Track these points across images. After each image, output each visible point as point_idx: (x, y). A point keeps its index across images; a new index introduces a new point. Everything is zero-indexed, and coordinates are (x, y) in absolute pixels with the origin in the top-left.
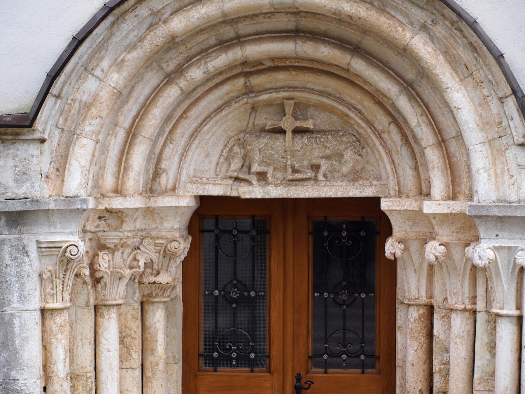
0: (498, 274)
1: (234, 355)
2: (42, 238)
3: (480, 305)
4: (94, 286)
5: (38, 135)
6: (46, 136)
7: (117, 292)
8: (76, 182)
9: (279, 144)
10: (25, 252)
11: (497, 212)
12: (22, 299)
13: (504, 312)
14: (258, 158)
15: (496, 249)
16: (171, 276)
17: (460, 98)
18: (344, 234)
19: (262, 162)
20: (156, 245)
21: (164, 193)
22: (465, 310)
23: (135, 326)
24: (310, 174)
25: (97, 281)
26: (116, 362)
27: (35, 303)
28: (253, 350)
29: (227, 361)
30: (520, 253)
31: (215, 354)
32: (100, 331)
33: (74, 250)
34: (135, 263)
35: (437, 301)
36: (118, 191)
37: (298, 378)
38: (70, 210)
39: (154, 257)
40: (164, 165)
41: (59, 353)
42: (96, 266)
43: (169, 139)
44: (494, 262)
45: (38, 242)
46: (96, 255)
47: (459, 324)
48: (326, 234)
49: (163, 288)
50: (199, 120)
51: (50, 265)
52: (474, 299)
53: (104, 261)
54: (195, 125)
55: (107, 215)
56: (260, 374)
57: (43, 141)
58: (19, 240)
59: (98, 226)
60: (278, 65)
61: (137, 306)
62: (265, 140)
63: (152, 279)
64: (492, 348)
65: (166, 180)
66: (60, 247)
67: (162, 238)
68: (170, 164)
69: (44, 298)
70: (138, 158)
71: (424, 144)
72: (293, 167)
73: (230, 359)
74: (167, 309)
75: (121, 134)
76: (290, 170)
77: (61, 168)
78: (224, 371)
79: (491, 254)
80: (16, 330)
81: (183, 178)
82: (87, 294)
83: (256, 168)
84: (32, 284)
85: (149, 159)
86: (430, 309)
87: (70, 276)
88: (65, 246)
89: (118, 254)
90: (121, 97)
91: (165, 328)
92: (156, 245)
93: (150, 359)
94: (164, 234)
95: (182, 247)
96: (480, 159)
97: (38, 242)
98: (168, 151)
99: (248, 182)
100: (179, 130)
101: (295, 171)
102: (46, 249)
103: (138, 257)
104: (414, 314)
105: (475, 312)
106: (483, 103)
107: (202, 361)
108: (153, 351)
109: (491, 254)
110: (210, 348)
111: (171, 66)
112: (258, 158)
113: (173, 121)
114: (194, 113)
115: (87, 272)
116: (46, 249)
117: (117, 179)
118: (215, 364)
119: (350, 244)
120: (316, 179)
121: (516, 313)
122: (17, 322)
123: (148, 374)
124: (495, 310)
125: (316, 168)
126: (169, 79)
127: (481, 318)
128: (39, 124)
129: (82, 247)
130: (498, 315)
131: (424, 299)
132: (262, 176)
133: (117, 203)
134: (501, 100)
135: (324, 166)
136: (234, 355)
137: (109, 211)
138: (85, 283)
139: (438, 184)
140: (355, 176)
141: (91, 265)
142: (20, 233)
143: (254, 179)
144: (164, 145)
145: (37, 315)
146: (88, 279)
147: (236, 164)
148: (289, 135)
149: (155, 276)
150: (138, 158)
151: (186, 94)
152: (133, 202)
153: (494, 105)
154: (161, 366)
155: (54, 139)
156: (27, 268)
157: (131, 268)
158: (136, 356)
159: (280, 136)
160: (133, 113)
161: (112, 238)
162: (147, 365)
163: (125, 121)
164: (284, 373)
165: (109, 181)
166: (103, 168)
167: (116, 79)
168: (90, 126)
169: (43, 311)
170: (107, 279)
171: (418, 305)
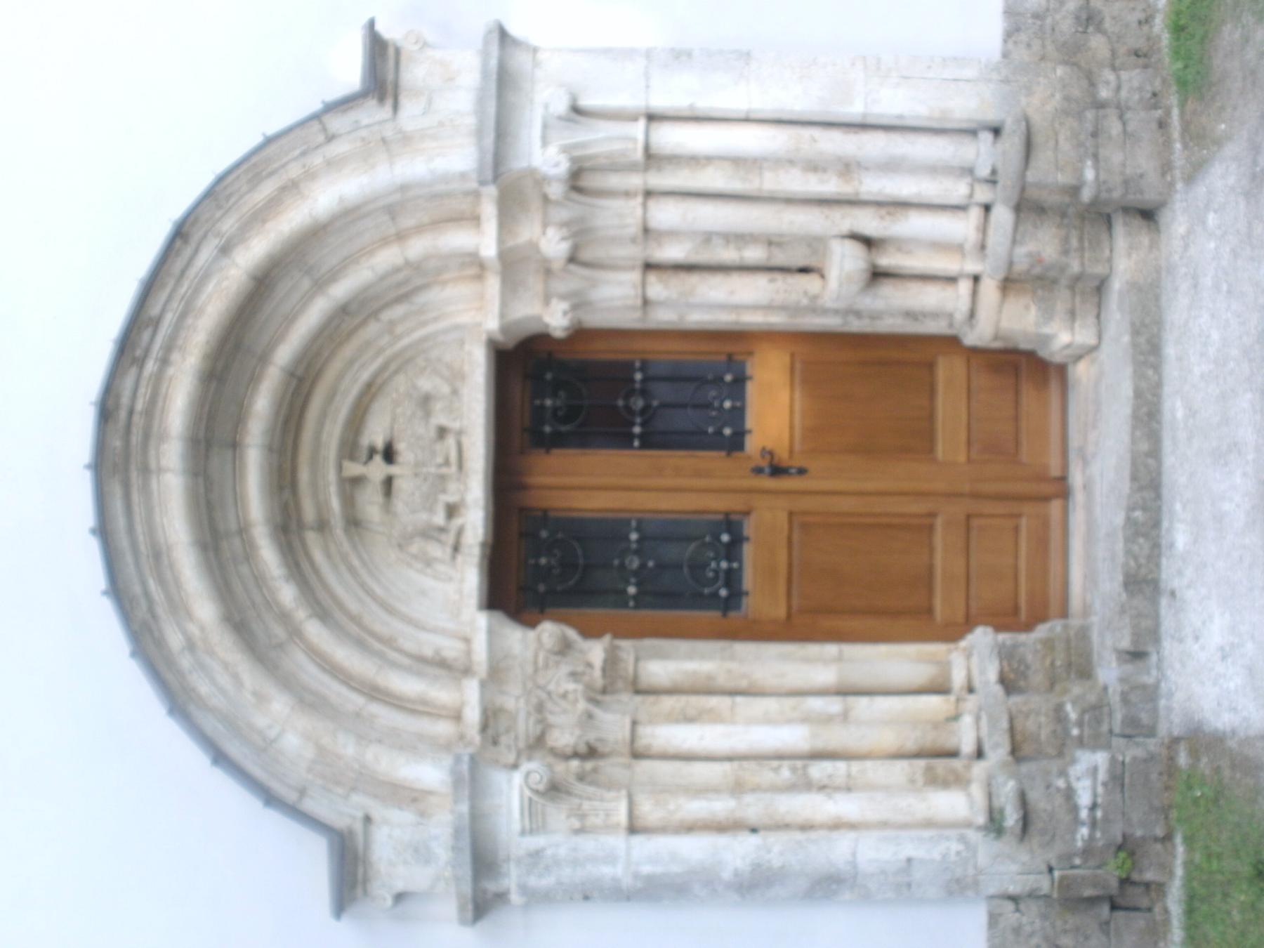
0: (583, 145)
1: (724, 565)
2: (516, 826)
3: (635, 181)
4: (602, 756)
5: (358, 827)
6: (360, 814)
7: (613, 725)
8: (430, 774)
9: (404, 486)
10: (536, 855)
11: (489, 140)
12: (611, 859)
13: (640, 137)
14: (423, 516)
15: (545, 142)
16: (596, 651)
17: (323, 198)
18: (548, 402)
19: (431, 510)
20: (546, 666)
21: (469, 653)
22: (644, 206)
23: (668, 702)
24: (451, 441)
25: (591, 753)
26: (719, 729)
27: (617, 841)
28: (717, 538)
29: (732, 579)
30: (551, 109)
31: (723, 592)
32: (671, 750)
33: (535, 777)
34: (571, 697)
35: (635, 253)
36: (457, 716)
37: (758, 471)
38: (471, 782)
39: (565, 669)
40: (428, 652)
41: (697, 808)
42: (569, 751)
43: (389, 642)
44: (565, 149)
45: (523, 833)
46: (554, 752)
47: (666, 214)
48: (547, 429)
49: (611, 662)
50: (368, 600)
51: (558, 816)
52: (627, 194)
53: (563, 738)
54: (374, 607)
55: (490, 732)
56: (749, 528)
57: (368, 819)
58: (519, 861)
59: (509, 747)
60: (283, 479)
61: (638, 699)
62: (399, 504)
63: (597, 673)
64: (696, 161)
65: (451, 649)
66: (530, 800)
67: (536, 656)
68: (429, 644)
69: (609, 828)
70: (407, 685)
71: (399, 261)
72: (440, 466)
73: (729, 572)
74: (651, 722)
75: (375, 708)
76: (444, 470)
77: (412, 797)
78: (748, 582)
79: (553, 150)
80: (659, 869)
81: (450, 626)
82: (612, 768)
83: (439, 519)
84: (588, 844)
85: (419, 674)
86: (649, 267)
87: (580, 788)
88: (528, 793)
89: (552, 719)
90: (310, 702)
91: (670, 662)
92: (546, 666)
93: (722, 681)
94: (529, 655)
95: (549, 631)
96: (413, 168)
97: (523, 833)
98: (409, 646)
99: (460, 532)
100: (378, 628)
101: (447, 463)
102: (534, 823)
103: (561, 691)
104: (657, 288)
105: (648, 194)
106: (332, 165)
107: (732, 614)
108: (710, 677)
109: (553, 150)
110: (711, 601)
111: (279, 632)
112: (423, 516)
113: (364, 638)
114: (353, 606)
115: (575, 764)
116: (534, 823)
117: (439, 716)
118: (736, 596)
119: (560, 391)
120: (460, 433)
121: (642, 123)
122: (646, 869)
123: (744, 684)
124: (639, 155)
125: (442, 432)
126: (296, 633)
127: (658, 180)
128: (340, 823)
129: (536, 768)
130: (647, 148)
131: (635, 276)
132: (452, 511)
133: (473, 715)
134: (330, 138)
135: (440, 419)
136: (724, 565)
137: (484, 727)
138: (595, 770)
139: (458, 239)
140: (456, 377)
141: (567, 757)
142: (508, 859)
143: (457, 522)
144: (400, 651)
145: (637, 840)
146: (589, 765)
147: (435, 550)
148: (393, 470)
149: (366, 463)
150: (407, 685)
151: (323, 615)
152: (471, 695)
153: (339, 148)
154: (733, 666)
155: (361, 802)
156: (562, 852)
157: (576, 701)
158: (714, 701)
159: (397, 484)
160: (344, 690)
161: (525, 726)
162: (731, 685)
163: (357, 700)
164: (750, 491)
165: (444, 728)
166: (421, 737)
167: (280, 704)
168: (347, 747)
169: (633, 829)
170: (591, 736)
171: (644, 284)
